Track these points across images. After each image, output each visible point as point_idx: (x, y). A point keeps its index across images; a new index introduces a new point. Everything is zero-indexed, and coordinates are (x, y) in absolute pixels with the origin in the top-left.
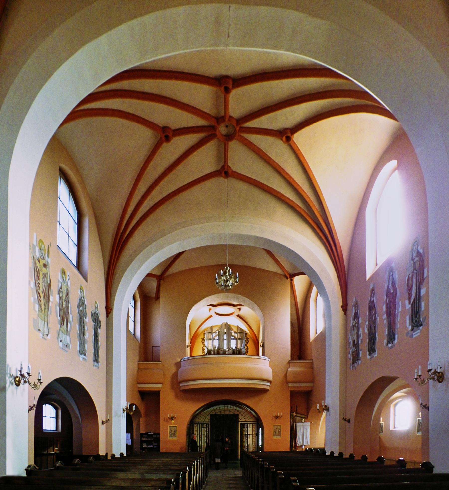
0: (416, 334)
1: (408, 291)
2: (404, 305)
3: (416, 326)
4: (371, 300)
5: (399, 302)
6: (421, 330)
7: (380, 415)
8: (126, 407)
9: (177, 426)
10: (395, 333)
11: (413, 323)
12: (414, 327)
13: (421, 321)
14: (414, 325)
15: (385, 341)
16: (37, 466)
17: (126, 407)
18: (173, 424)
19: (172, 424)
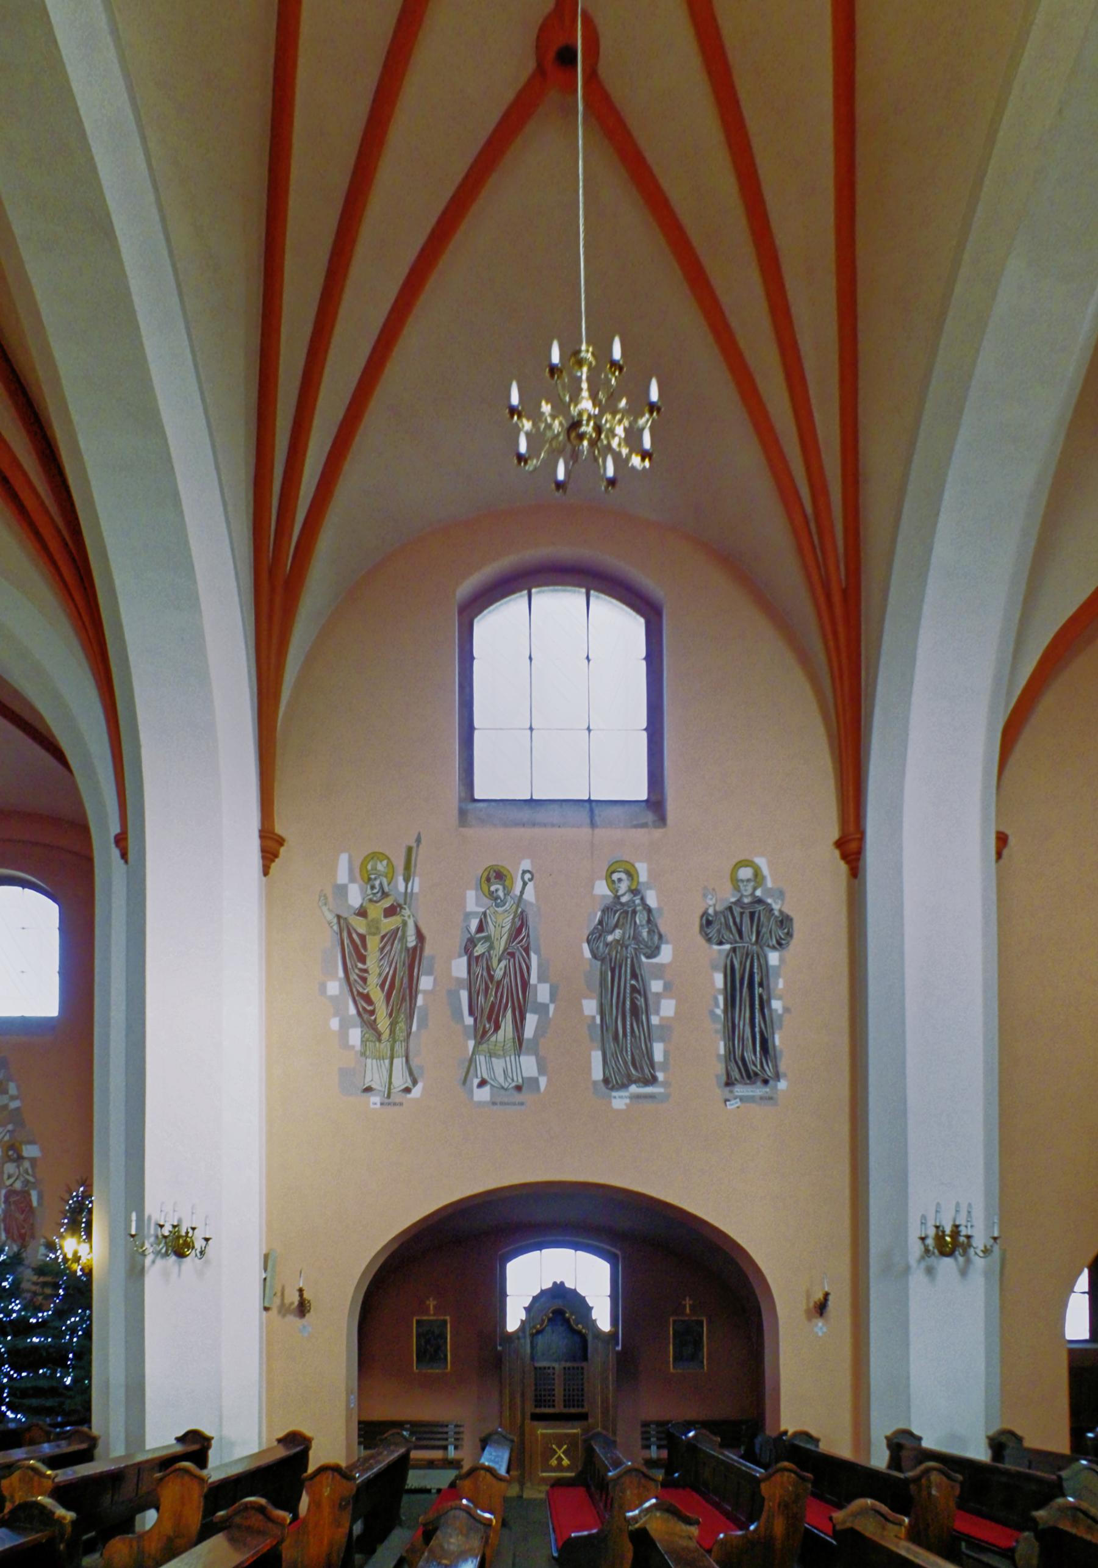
9: (448, 1318)
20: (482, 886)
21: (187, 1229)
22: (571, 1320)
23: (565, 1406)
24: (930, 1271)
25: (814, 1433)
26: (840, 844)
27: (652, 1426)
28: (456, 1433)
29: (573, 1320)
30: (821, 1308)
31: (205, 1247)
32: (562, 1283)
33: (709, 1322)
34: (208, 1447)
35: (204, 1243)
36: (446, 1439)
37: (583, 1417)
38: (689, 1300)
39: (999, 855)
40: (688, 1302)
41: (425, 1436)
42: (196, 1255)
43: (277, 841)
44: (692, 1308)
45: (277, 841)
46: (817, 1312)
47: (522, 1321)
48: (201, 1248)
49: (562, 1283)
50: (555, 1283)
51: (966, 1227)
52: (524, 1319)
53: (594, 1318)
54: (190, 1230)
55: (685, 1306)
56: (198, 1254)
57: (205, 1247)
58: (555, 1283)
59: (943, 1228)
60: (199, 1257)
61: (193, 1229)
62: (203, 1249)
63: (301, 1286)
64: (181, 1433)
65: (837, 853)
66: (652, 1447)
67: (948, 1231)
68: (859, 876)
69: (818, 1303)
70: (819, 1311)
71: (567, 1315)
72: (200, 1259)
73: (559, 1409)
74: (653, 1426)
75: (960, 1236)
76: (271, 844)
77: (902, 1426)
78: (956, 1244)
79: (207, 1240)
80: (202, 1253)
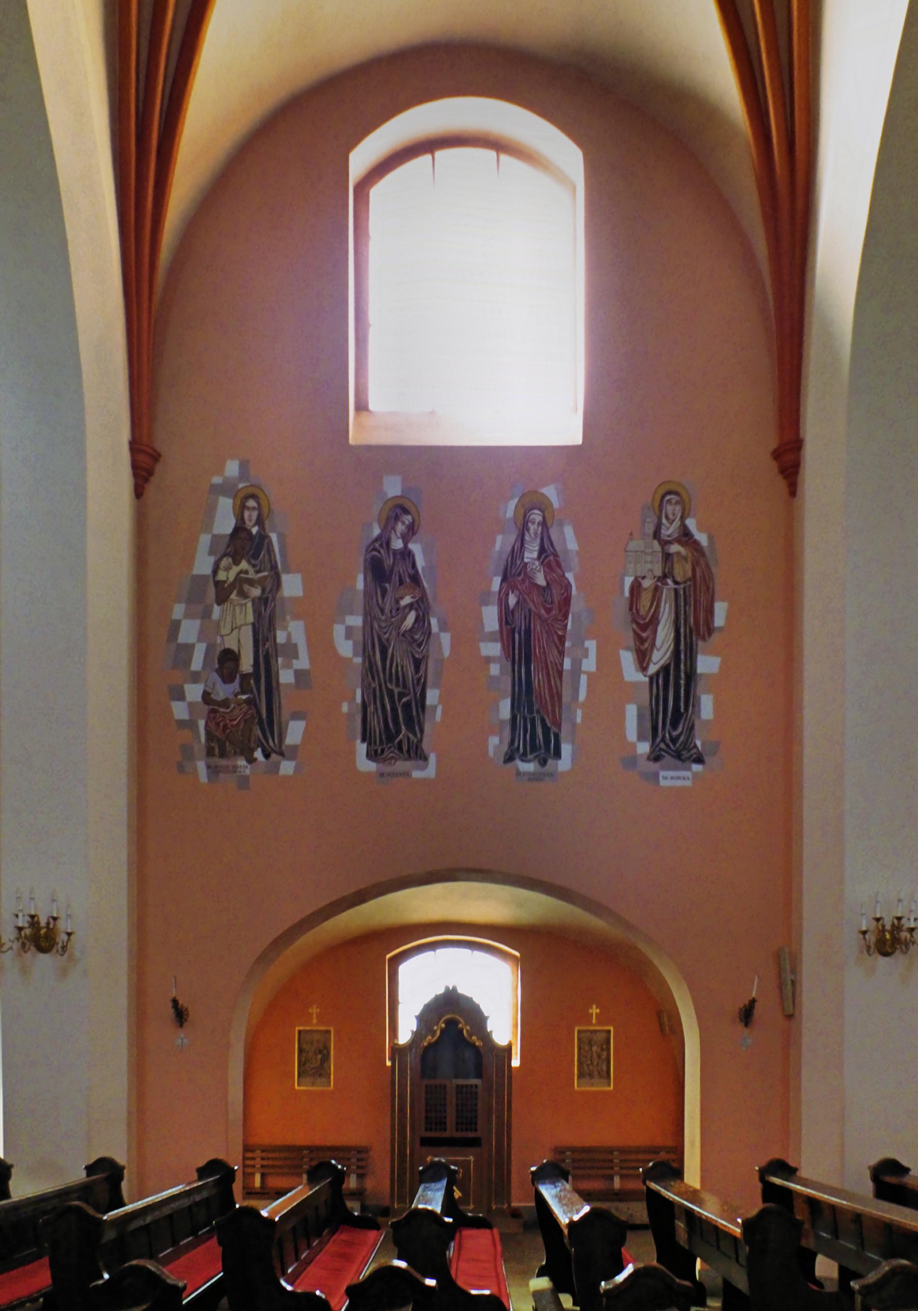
0: (672, 778)
1: (638, 643)
2: (608, 662)
3: (244, 608)
4: (384, 541)
5: (579, 643)
6: (695, 775)
7: (537, 1207)
8: (897, 928)
9: (612, 1029)
10: (557, 737)
11: (658, 740)
12: (663, 753)
13: (695, 746)
14: (662, 746)
15: (495, 744)
16: (280, 1218)
17: (897, 928)
18: (594, 1021)
19: (591, 1024)
20: (267, 512)
21: (48, 920)
22: (465, 1032)
23: (457, 1130)
24: (24, 971)
25: (905, 1163)
26: (777, 455)
27: (615, 1153)
28: (358, 1160)
29: (467, 1031)
30: (747, 1015)
31: (67, 943)
32: (454, 989)
33: (337, 1033)
34: (121, 1178)
35: (65, 937)
36: (612, 1168)
37: (475, 1143)
38: (596, 1008)
39: (139, 492)
40: (594, 1011)
41: (281, 1163)
42: (57, 951)
43: (151, 456)
44: (320, 1016)
45: (151, 456)
46: (741, 1020)
47: (413, 1032)
48: (63, 943)
49: (454, 989)
50: (447, 988)
51: (909, 919)
52: (415, 1030)
53: (489, 1030)
54: (51, 920)
55: (311, 1014)
56: (60, 950)
57: (67, 943)
58: (447, 988)
59: (38, 919)
60: (61, 953)
61: (55, 919)
62: (65, 944)
63: (754, 995)
64: (202, 1162)
65: (774, 466)
66: (615, 1178)
67: (888, 927)
68: (798, 493)
69: (744, 1010)
70: (744, 1020)
71: (460, 1026)
72: (62, 955)
73: (450, 1132)
74: (568, 1153)
75: (902, 931)
76: (143, 459)
77: (778, 1156)
78: (896, 941)
79: (69, 934)
80: (64, 948)
